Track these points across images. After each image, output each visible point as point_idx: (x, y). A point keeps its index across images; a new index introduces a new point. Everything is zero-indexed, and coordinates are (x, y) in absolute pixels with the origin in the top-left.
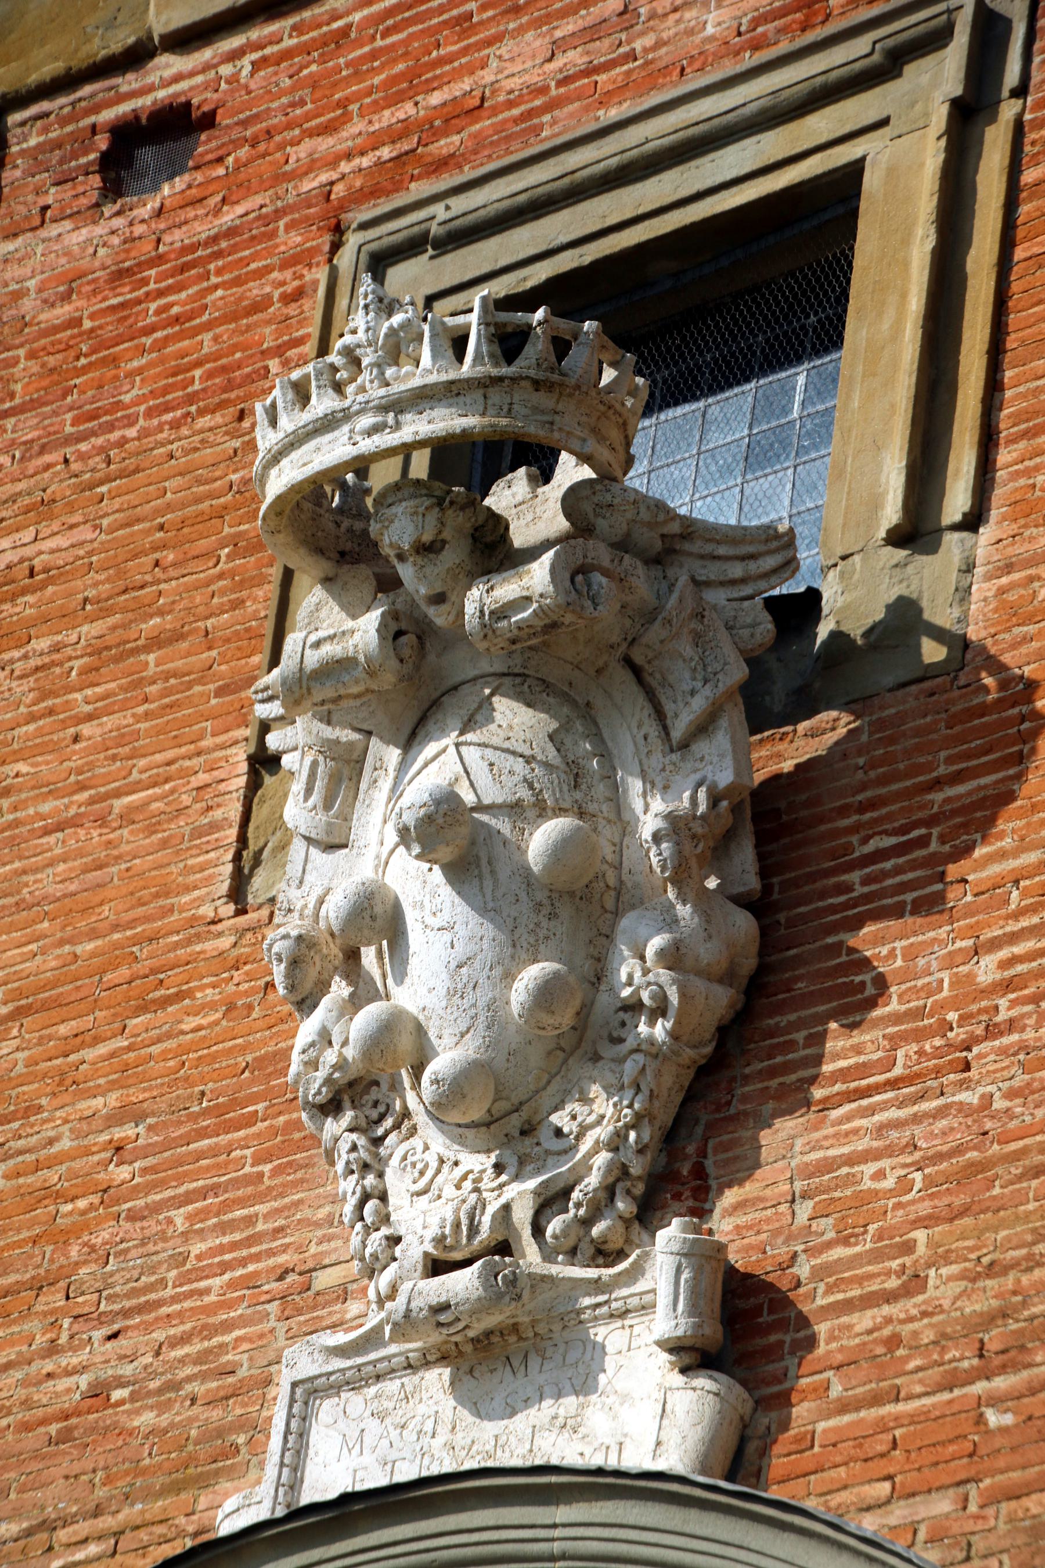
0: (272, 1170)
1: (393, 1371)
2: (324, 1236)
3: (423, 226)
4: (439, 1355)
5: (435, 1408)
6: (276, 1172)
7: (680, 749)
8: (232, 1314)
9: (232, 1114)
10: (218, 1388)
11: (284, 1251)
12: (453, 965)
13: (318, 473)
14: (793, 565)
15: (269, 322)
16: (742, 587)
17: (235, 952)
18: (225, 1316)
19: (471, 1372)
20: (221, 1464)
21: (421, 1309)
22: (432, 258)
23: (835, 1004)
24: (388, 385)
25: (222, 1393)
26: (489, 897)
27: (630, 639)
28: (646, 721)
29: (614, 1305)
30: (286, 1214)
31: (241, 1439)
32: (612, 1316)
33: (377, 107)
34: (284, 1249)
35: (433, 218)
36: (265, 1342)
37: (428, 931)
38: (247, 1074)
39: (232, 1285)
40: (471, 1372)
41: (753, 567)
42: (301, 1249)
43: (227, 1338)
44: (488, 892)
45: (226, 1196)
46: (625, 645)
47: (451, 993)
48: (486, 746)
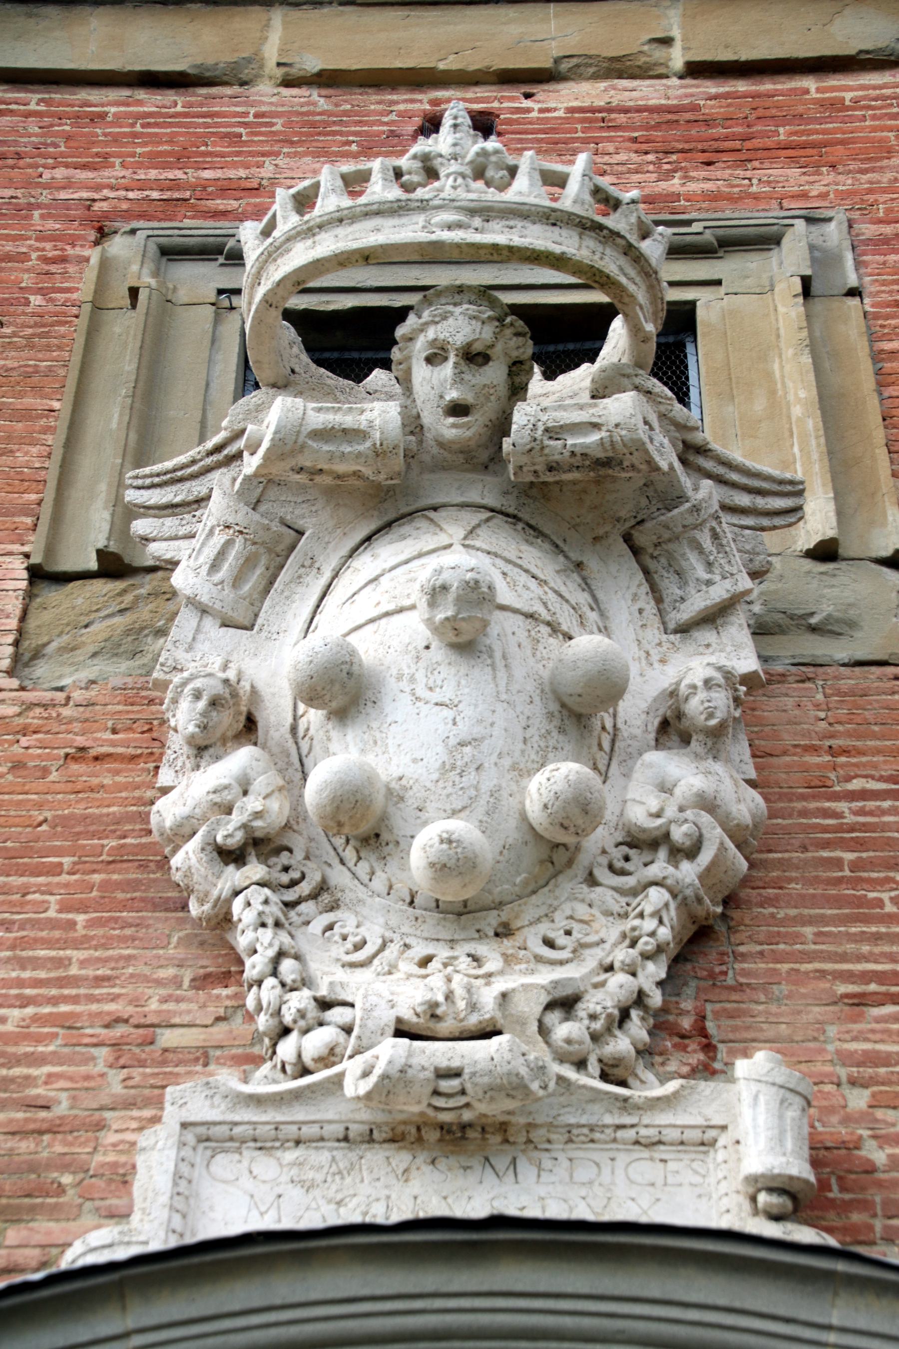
0: (88, 921)
1: (322, 1139)
2: (170, 996)
3: (219, 239)
4: (389, 1135)
5: (387, 1192)
6: (90, 924)
7: (676, 632)
8: (41, 1049)
9: (26, 860)
10: (27, 1120)
11: (112, 1000)
12: (453, 741)
13: (381, 246)
14: (799, 515)
15: (27, 271)
16: (743, 517)
17: (21, 721)
18: (30, 1049)
19: (433, 1162)
20: (39, 1200)
21: (423, 1068)
22: (222, 265)
23: (847, 911)
24: (669, 98)
25: (32, 1126)
26: (502, 688)
27: (639, 519)
28: (643, 597)
29: (643, 1132)
30: (113, 965)
31: (67, 1179)
32: (637, 1142)
33: (140, 165)
34: (115, 998)
35: (234, 236)
36: (92, 1084)
37: (418, 704)
38: (44, 827)
39: (36, 1019)
40: (433, 1162)
41: (761, 502)
42: (136, 1001)
43: (34, 1072)
44: (502, 683)
45: (24, 933)
46: (633, 522)
47: (445, 769)
48: (496, 555)
